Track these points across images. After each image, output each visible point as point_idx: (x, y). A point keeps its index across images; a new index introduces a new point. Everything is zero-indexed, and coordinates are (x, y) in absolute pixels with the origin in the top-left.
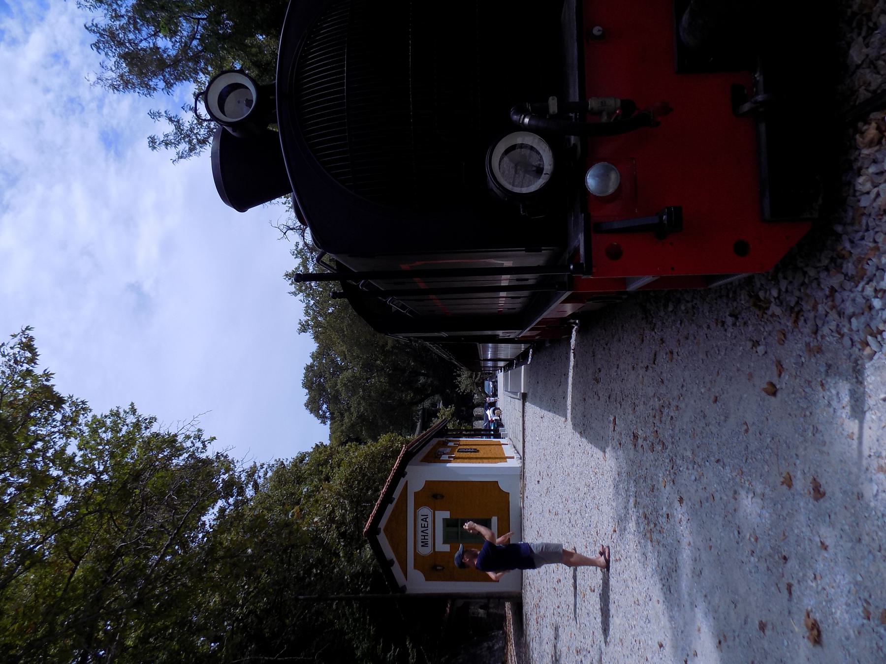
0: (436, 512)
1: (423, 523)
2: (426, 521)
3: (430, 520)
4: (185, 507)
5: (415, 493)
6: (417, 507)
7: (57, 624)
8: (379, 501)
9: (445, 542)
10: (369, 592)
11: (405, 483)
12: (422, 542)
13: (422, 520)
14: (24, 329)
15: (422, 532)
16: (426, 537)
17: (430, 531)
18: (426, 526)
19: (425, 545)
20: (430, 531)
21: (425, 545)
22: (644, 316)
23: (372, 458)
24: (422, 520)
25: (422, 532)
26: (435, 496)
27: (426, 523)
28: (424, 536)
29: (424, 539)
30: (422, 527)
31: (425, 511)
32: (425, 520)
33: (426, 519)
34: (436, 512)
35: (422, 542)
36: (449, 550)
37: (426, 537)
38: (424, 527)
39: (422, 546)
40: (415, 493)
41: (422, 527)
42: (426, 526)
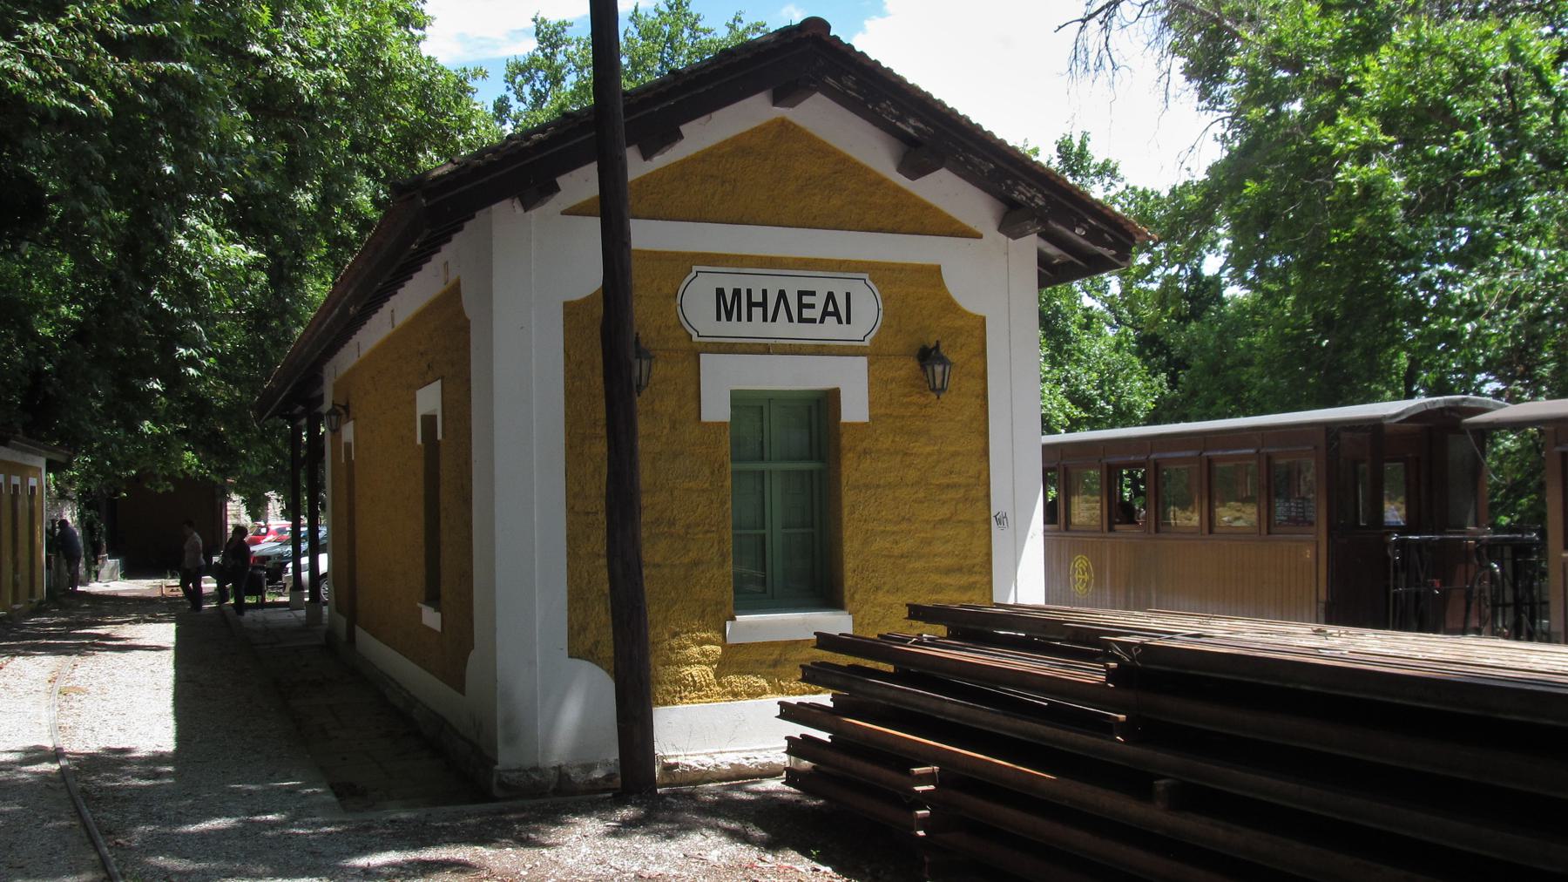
0: (862, 362)
1: (819, 301)
2: (825, 313)
3: (830, 330)
4: (363, 115)
5: (935, 271)
6: (879, 273)
7: (508, 116)
8: (480, 182)
9: (742, 402)
10: (1083, 237)
11: (979, 229)
12: (737, 293)
13: (831, 296)
14: (731, 23)
15: (782, 295)
16: (757, 312)
17: (782, 329)
18: (807, 313)
19: (727, 306)
20: (782, 329)
21: (727, 306)
22: (1282, 53)
23: (1287, 135)
24: (831, 296)
25: (782, 295)
26: (928, 356)
27: (816, 313)
28: (764, 305)
29: (751, 305)
30: (801, 294)
31: (867, 312)
32: (831, 310)
33: (836, 313)
34: (862, 362)
35: (737, 293)
36: (707, 416)
37: (757, 312)
38: (801, 306)
39: (720, 293)
40: (935, 271)
41: (801, 294)
42: (807, 313)
